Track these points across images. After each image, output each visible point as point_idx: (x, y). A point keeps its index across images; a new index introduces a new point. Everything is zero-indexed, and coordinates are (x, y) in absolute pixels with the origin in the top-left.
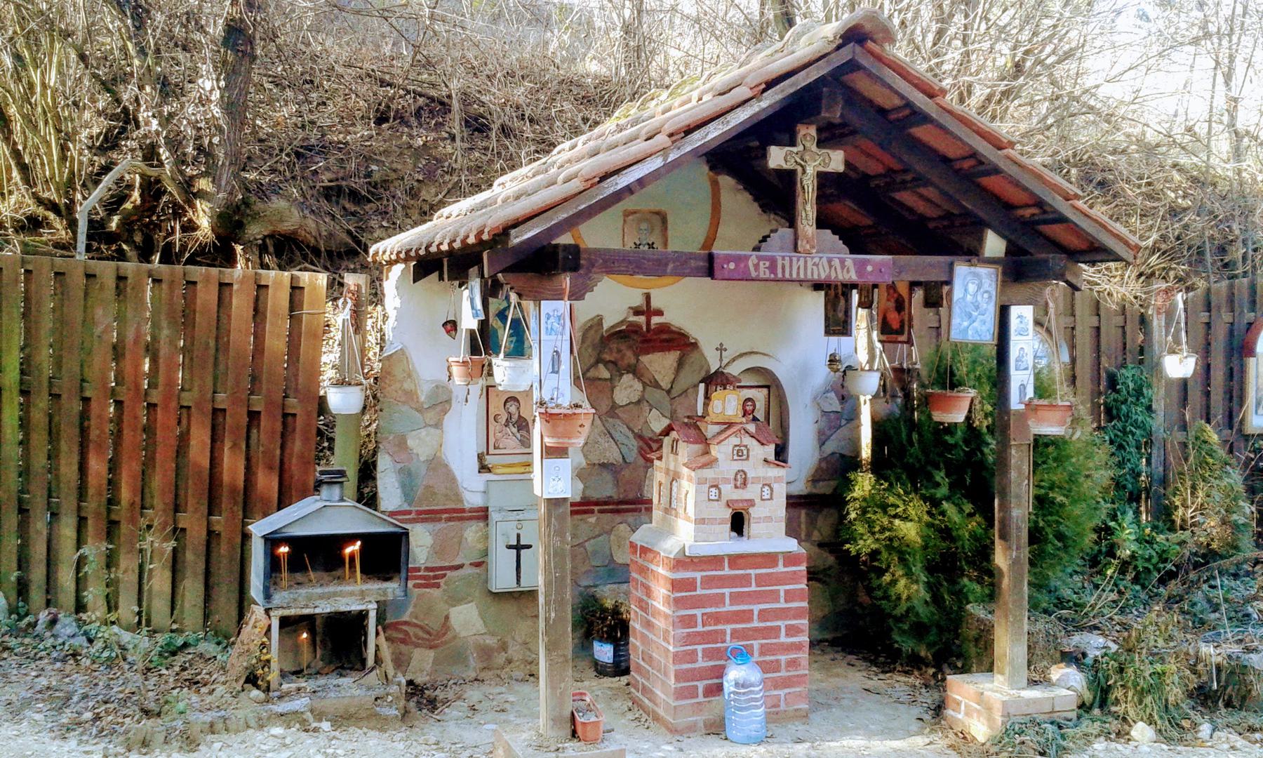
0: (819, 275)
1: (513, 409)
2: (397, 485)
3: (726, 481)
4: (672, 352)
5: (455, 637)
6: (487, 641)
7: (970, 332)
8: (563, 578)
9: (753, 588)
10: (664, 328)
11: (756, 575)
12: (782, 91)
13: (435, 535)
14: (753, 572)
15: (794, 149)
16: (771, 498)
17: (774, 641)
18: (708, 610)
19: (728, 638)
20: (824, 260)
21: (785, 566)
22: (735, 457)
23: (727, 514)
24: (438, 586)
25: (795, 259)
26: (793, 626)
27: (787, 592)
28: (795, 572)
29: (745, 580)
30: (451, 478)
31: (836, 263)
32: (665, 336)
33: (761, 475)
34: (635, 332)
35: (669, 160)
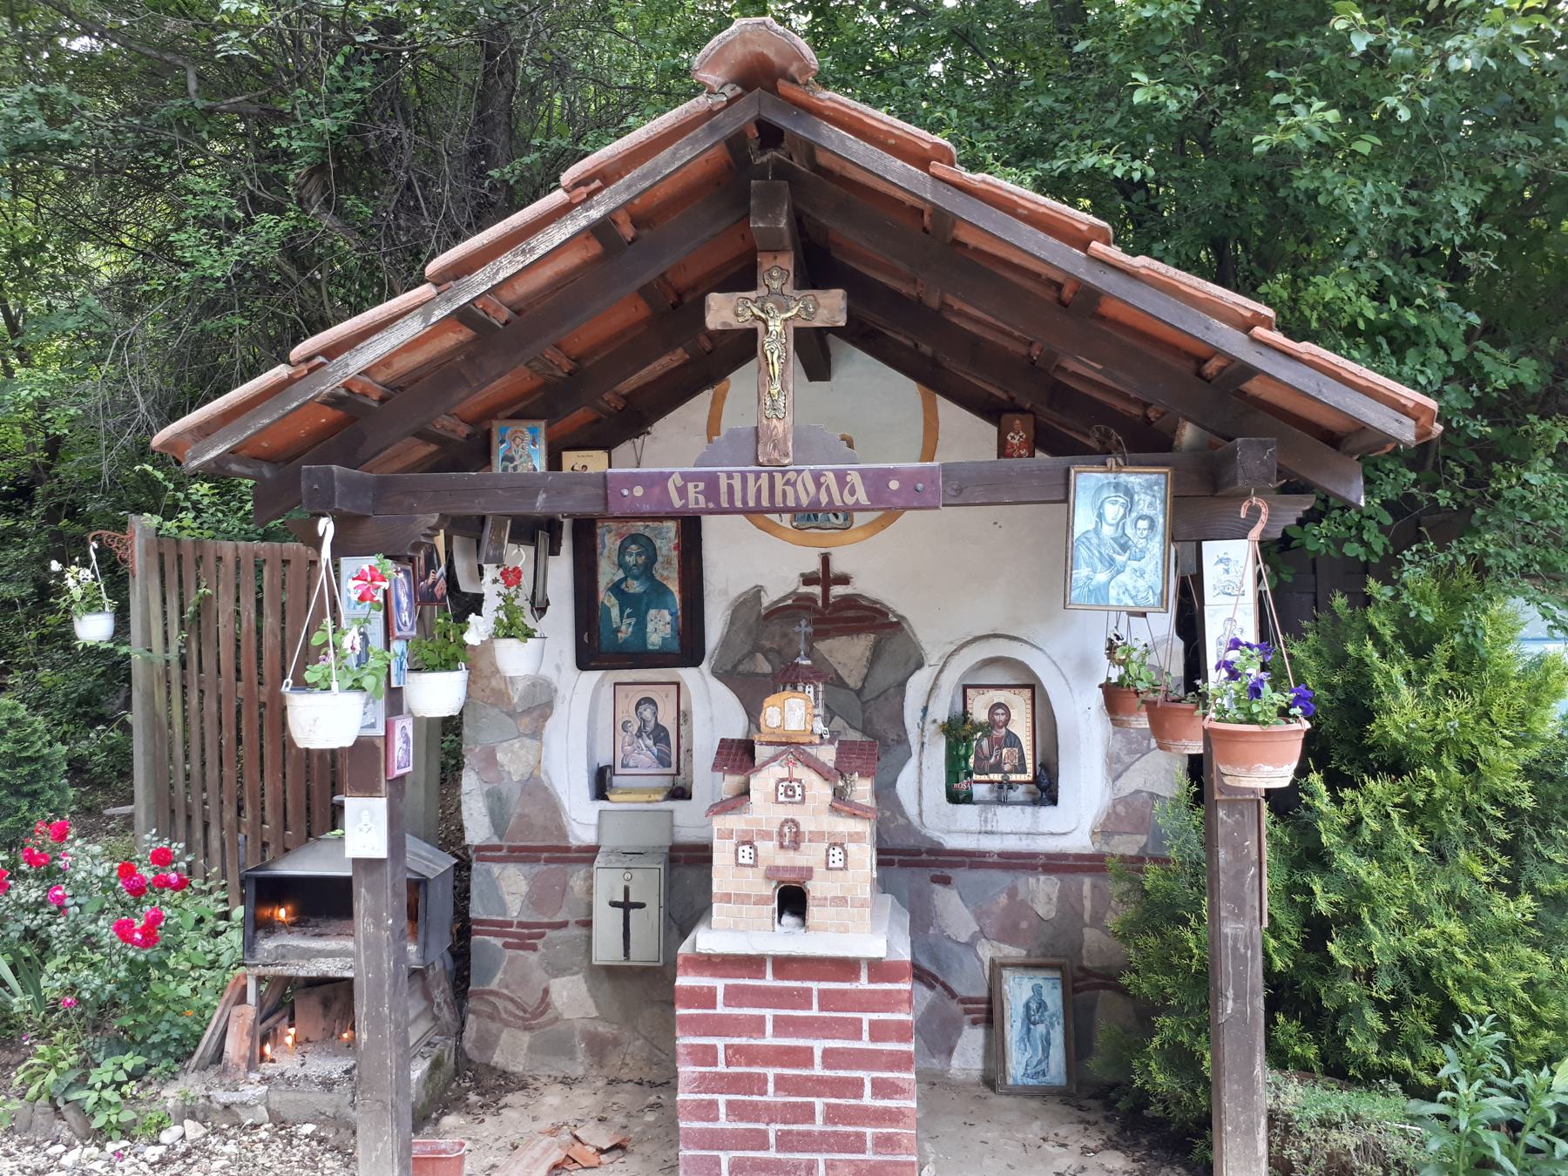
0: (797, 498)
1: (648, 714)
2: (484, 811)
3: (766, 835)
4: (863, 636)
5: (556, 1019)
6: (600, 1029)
7: (1113, 593)
8: (380, 985)
9: (815, 1012)
10: (850, 601)
11: (821, 992)
12: (629, 187)
13: (533, 881)
14: (815, 986)
15: (752, 295)
16: (845, 868)
17: (852, 1102)
18: (736, 1041)
19: (771, 1087)
20: (807, 476)
21: (871, 980)
22: (782, 798)
23: (770, 890)
24: (534, 948)
25: (751, 478)
26: (884, 1081)
27: (872, 1024)
28: (888, 993)
29: (803, 998)
30: (553, 807)
31: (830, 479)
32: (851, 613)
33: (826, 828)
34: (807, 608)
35: (433, 320)
